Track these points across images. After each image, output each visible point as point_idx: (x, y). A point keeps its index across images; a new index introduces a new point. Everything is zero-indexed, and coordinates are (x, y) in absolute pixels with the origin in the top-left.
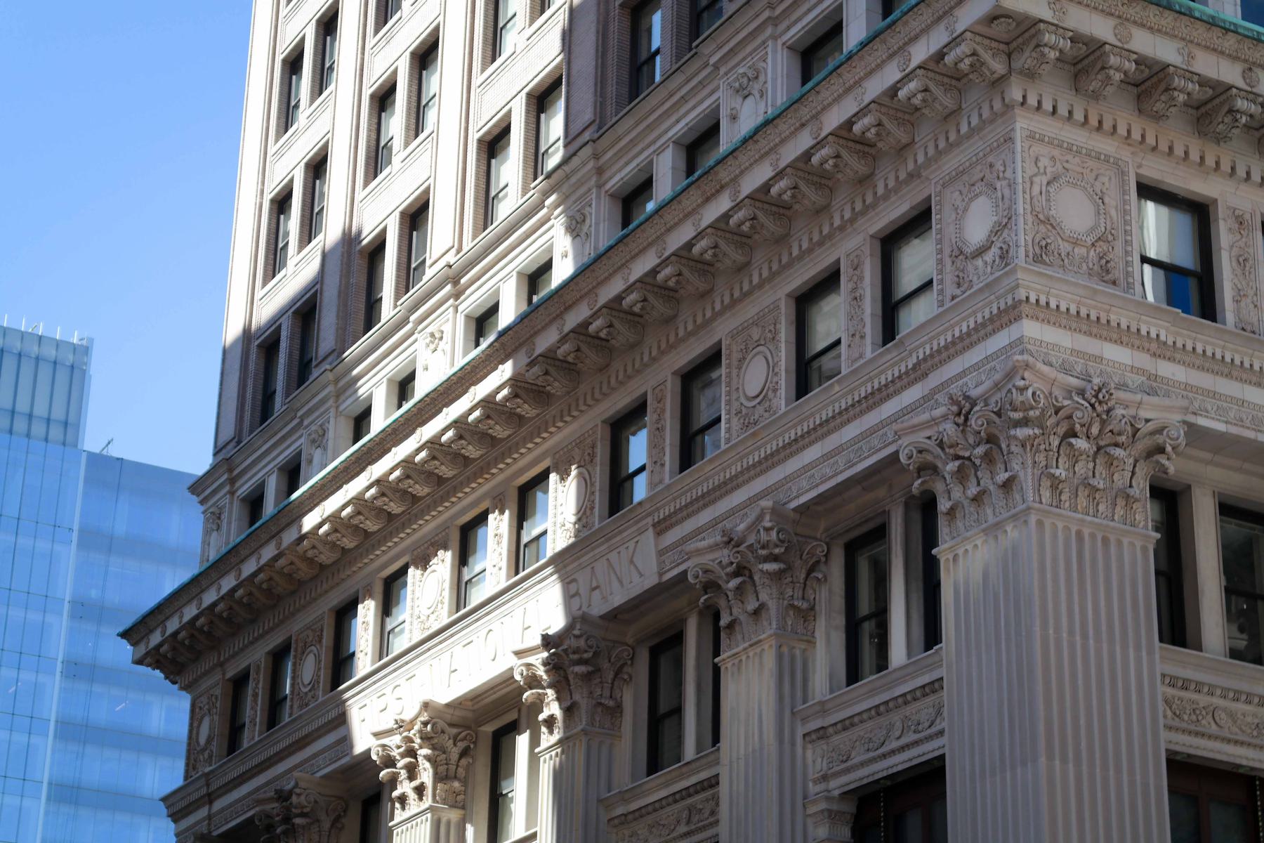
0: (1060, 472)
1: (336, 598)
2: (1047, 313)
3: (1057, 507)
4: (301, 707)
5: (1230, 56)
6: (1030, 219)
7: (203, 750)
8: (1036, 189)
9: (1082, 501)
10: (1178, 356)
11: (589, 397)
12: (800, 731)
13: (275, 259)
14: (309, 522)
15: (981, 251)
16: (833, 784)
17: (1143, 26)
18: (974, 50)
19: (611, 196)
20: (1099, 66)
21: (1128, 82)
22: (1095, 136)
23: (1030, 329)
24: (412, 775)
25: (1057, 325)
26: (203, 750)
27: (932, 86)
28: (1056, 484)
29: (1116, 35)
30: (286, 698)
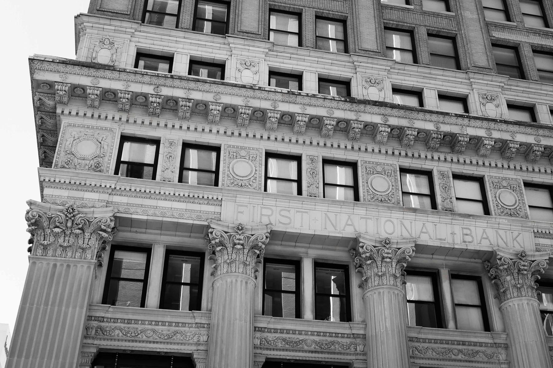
3: (45, 256)
5: (147, 84)
9: (59, 252)
10: (168, 198)
18: (40, 98)
20: (507, 148)
21: (493, 148)
22: (99, 121)
25: (56, 188)
29: (536, 141)
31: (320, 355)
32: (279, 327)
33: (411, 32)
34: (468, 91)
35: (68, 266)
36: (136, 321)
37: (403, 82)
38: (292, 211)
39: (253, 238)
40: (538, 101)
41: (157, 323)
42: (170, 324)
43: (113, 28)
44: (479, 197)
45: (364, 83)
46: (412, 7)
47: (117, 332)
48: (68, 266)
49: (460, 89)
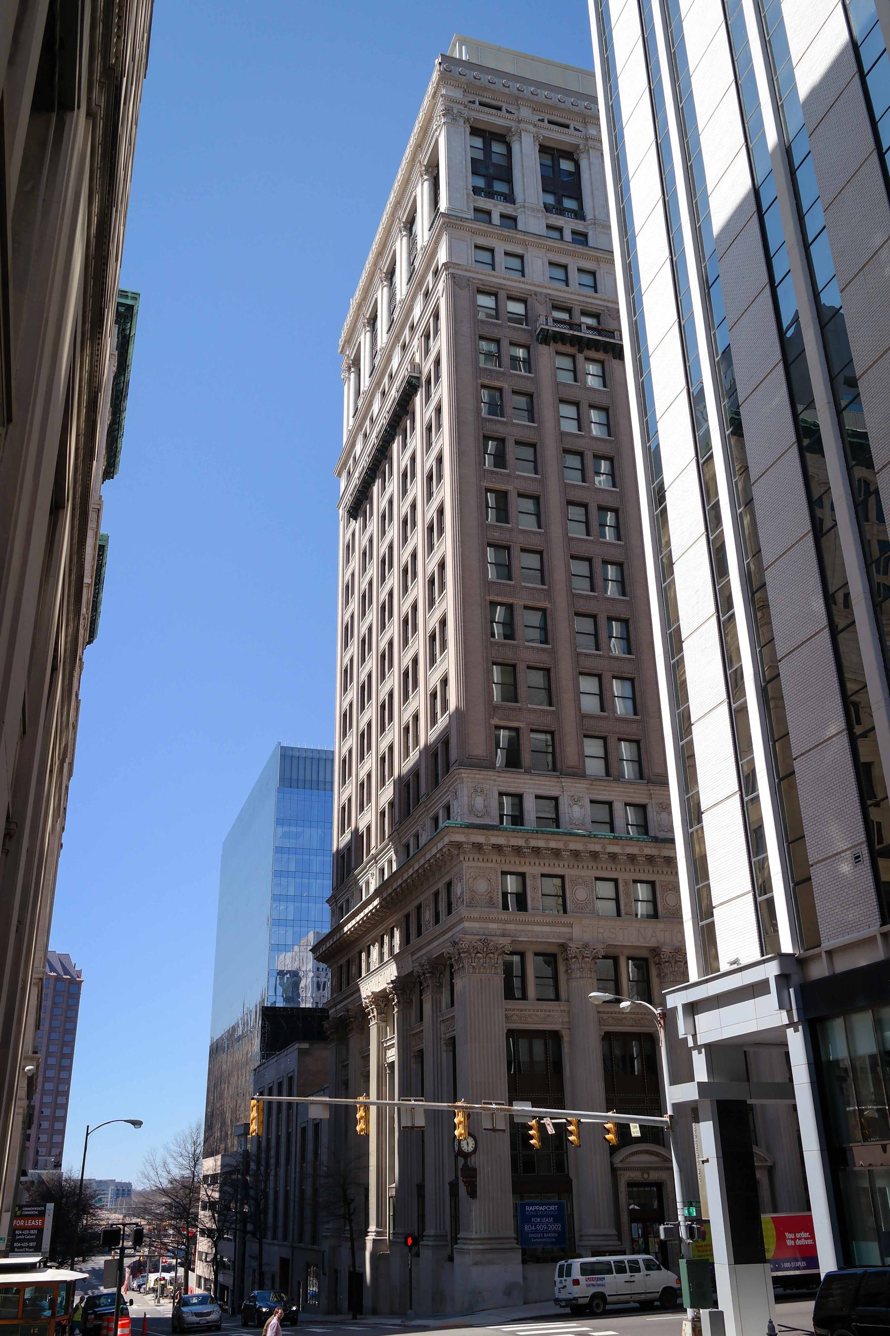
0: (474, 964)
1: (357, 950)
2: (470, 919)
6: (468, 891)
7: (460, 898)
12: (439, 1021)
13: (434, 721)
14: (346, 929)
16: (447, 1035)
23: (466, 924)
24: (373, 1013)
26: (460, 898)
31: (636, 1028)
32: (610, 1010)
35: (489, 980)
36: (526, 1010)
39: (595, 951)
41: (538, 1011)
42: (545, 1011)
43: (482, 777)
44: (490, 262)
46: (583, 433)
47: (515, 1017)
48: (489, 980)
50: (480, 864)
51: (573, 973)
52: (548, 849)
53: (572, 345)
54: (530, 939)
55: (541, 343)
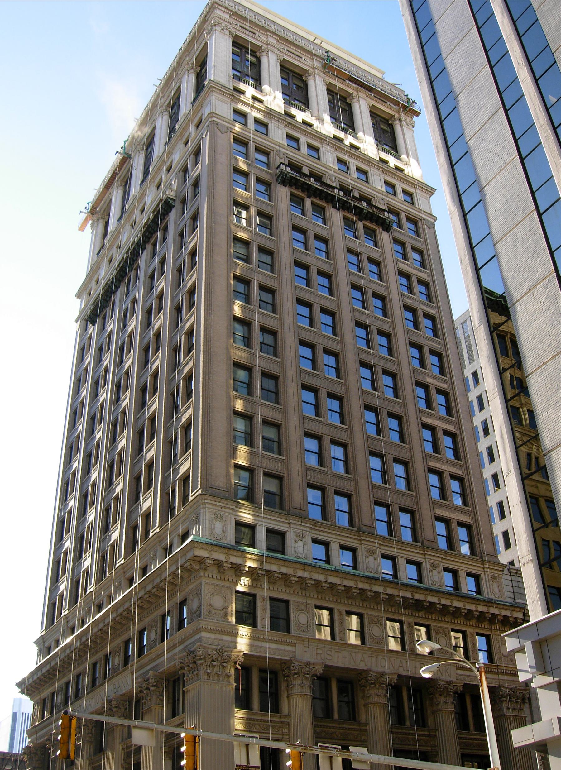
3: (222, 681)
4: (115, 672)
8: (207, 597)
11: (198, 575)
15: (195, 612)
17: (233, 555)
19: (127, 579)
27: (192, 563)
28: (208, 674)
30: (129, 656)
33: (323, 490)
34: (287, 529)
37: (387, 552)
38: (333, 651)
40: (461, 568)
45: (366, 553)
49: (419, 558)
50: (217, 582)
51: (294, 688)
52: (279, 573)
53: (303, 191)
54: (259, 654)
55: (279, 183)
